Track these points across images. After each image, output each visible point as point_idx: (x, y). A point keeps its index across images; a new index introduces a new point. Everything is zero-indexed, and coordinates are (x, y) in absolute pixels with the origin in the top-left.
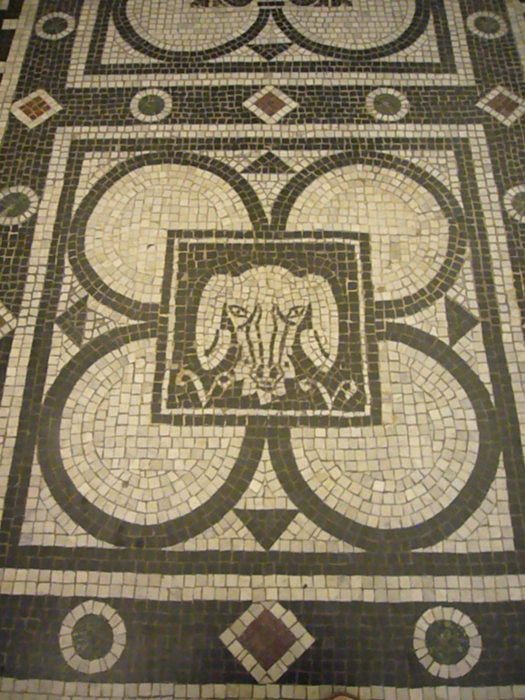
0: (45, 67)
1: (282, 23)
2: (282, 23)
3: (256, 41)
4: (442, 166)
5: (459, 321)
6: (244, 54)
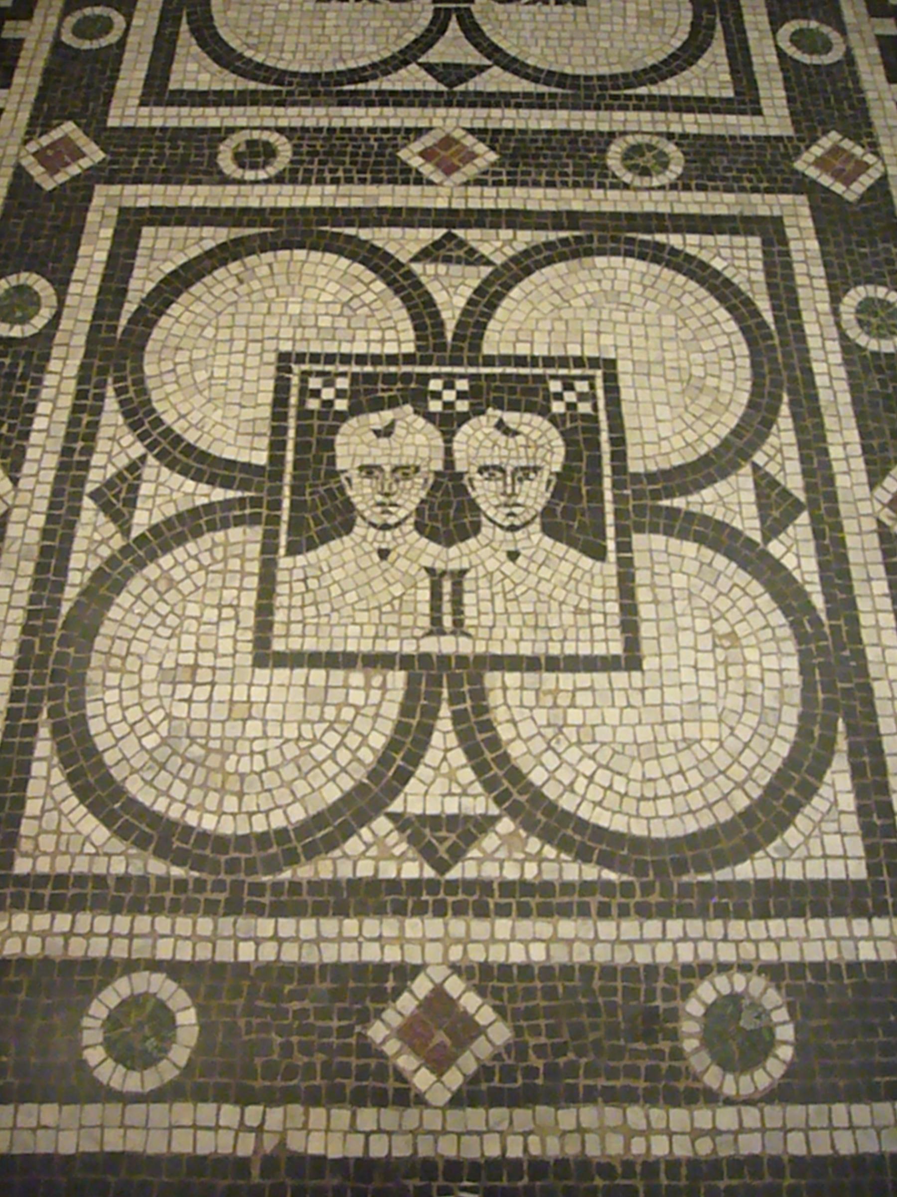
0: (76, 86)
1: (473, 32)
2: (473, 32)
3: (433, 56)
4: (740, 260)
6: (411, 78)
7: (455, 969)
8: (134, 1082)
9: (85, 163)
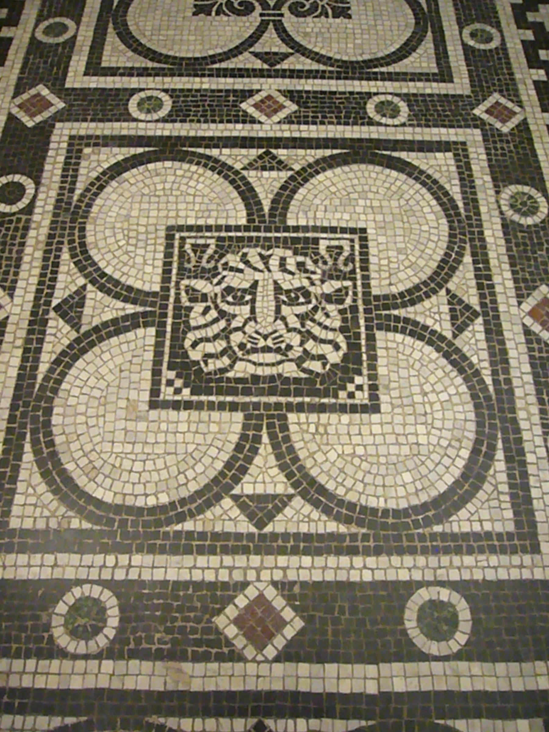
0: (45, 64)
3: (257, 48)
4: (441, 166)
5: (461, 315)
7: (274, 584)
8: (81, 648)
9: (53, 110)
